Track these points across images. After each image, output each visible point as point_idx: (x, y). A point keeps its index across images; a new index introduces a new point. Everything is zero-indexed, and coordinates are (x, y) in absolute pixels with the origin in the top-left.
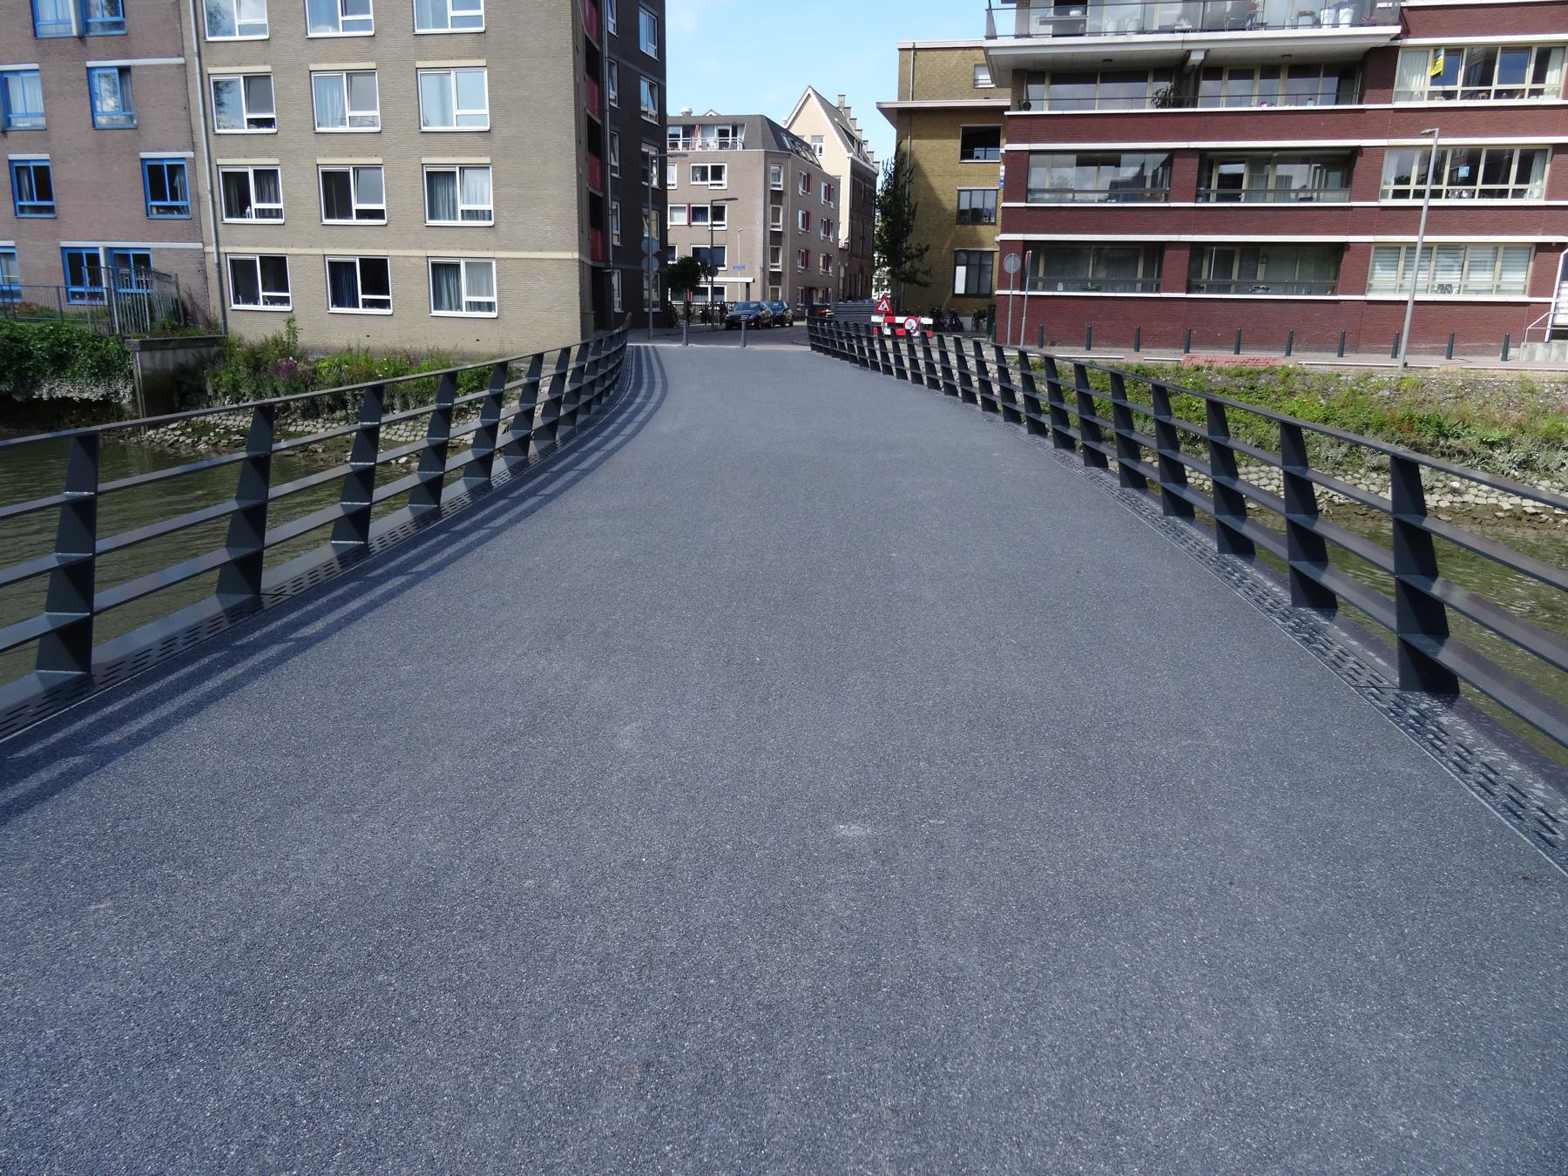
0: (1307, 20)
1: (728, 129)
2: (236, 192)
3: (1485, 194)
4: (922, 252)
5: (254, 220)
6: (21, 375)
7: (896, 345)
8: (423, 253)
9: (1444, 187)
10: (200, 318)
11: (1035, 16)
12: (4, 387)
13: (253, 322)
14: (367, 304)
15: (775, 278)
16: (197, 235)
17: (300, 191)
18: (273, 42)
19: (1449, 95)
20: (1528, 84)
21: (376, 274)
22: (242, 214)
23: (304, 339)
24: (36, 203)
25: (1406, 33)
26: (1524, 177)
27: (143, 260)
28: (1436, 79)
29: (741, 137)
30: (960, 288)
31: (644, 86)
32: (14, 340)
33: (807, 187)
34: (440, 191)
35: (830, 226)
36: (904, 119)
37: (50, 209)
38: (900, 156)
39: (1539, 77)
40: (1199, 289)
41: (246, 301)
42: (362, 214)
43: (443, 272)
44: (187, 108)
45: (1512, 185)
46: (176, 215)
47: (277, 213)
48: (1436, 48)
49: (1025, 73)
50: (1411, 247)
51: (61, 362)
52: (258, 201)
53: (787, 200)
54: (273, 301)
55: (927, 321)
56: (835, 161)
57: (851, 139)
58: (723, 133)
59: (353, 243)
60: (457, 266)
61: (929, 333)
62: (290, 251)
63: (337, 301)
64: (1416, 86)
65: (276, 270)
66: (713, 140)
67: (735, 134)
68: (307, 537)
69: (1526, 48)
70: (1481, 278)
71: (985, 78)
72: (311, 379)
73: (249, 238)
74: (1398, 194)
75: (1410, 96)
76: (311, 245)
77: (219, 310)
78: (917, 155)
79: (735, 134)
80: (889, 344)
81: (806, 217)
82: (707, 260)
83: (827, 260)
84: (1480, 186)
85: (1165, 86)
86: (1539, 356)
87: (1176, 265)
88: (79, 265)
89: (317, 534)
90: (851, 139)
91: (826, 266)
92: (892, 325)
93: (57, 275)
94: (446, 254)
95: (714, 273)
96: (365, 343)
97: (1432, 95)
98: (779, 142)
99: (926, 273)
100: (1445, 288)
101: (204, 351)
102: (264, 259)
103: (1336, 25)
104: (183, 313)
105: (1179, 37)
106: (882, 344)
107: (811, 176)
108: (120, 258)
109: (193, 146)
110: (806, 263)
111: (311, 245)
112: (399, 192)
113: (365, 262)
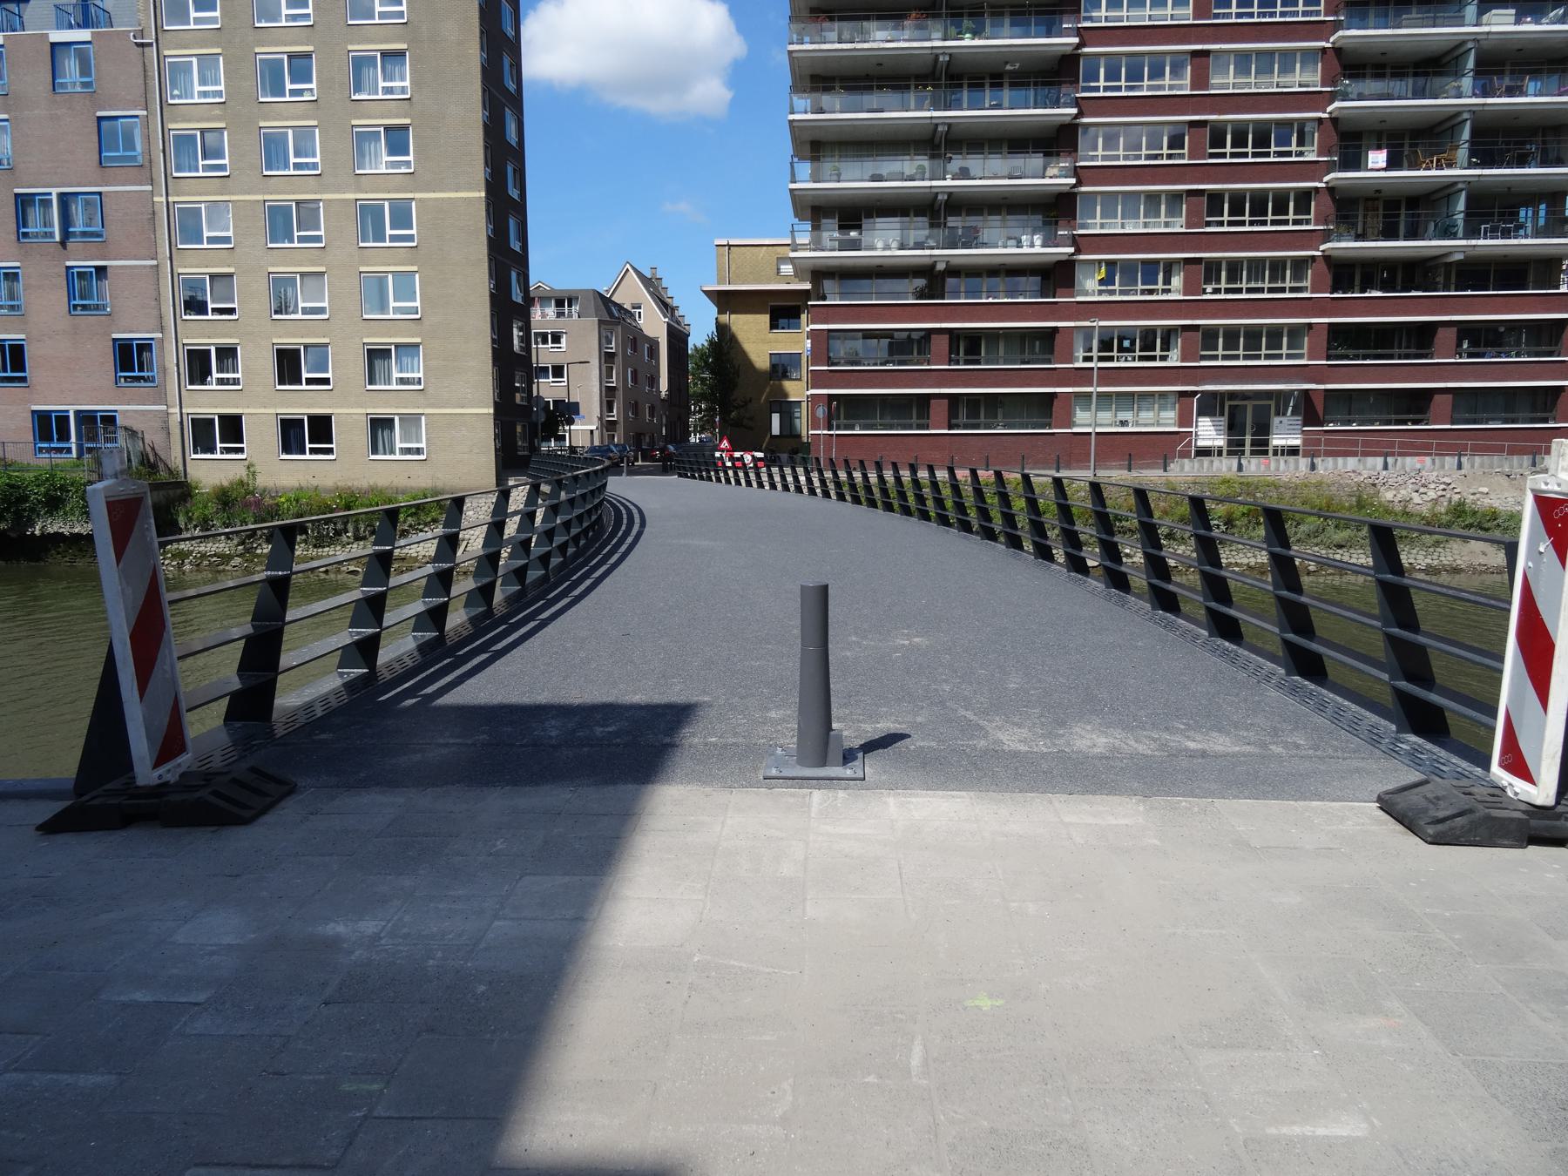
0: (1013, 242)
1: (562, 301)
2: (198, 365)
3: (1142, 358)
4: (747, 402)
5: (214, 387)
6: (18, 515)
7: (736, 474)
8: (364, 411)
9: (1115, 354)
10: (161, 466)
11: (826, 235)
12: (3, 526)
13: (210, 471)
14: (313, 451)
15: (610, 426)
16: (162, 398)
17: (256, 363)
18: (237, 250)
19: (1112, 292)
20: (1160, 286)
21: (321, 428)
22: (203, 382)
23: (262, 481)
24: (9, 374)
25: (1078, 251)
26: (1166, 347)
27: (110, 420)
28: (1101, 282)
29: (575, 308)
30: (776, 430)
31: (514, 275)
32: (12, 486)
33: (635, 349)
34: (378, 363)
35: (654, 380)
36: (726, 301)
37: (24, 379)
38: (722, 329)
39: (1167, 281)
40: (958, 427)
41: (204, 451)
42: (310, 381)
43: (380, 426)
44: (158, 299)
45: (1158, 353)
46: (143, 384)
47: (236, 382)
48: (1100, 261)
49: (820, 274)
50: (1089, 395)
51: (54, 504)
52: (220, 370)
53: (619, 359)
54: (229, 450)
55: (760, 455)
56: (653, 324)
57: (666, 307)
58: (560, 303)
59: (301, 403)
60: (392, 420)
61: (760, 464)
62: (246, 411)
63: (287, 449)
64: (1090, 287)
65: (232, 427)
66: (551, 311)
67: (570, 305)
68: (326, 617)
69: (1157, 261)
70: (1146, 415)
71: (787, 269)
72: (274, 512)
73: (209, 401)
74: (1087, 359)
75: (1087, 294)
76: (263, 404)
77: (179, 461)
78: (734, 328)
79: (570, 305)
80: (731, 473)
81: (635, 373)
82: (567, 411)
83: (652, 409)
84: (1138, 353)
85: (920, 282)
86: (1187, 468)
87: (939, 410)
88: (48, 426)
89: (336, 615)
90: (666, 307)
91: (652, 415)
92: (732, 459)
93: (24, 430)
94: (382, 411)
95: (571, 422)
96: (315, 482)
97: (1100, 292)
98: (612, 314)
99: (751, 419)
100: (1123, 423)
101: (171, 492)
102: (221, 417)
103: (1032, 245)
104: (150, 464)
105: (928, 252)
106: (726, 474)
107: (637, 341)
108: (86, 418)
109: (162, 329)
110: (636, 413)
111: (263, 404)
112: (345, 364)
113: (312, 418)
